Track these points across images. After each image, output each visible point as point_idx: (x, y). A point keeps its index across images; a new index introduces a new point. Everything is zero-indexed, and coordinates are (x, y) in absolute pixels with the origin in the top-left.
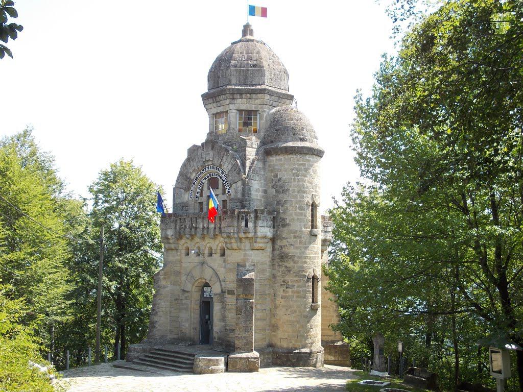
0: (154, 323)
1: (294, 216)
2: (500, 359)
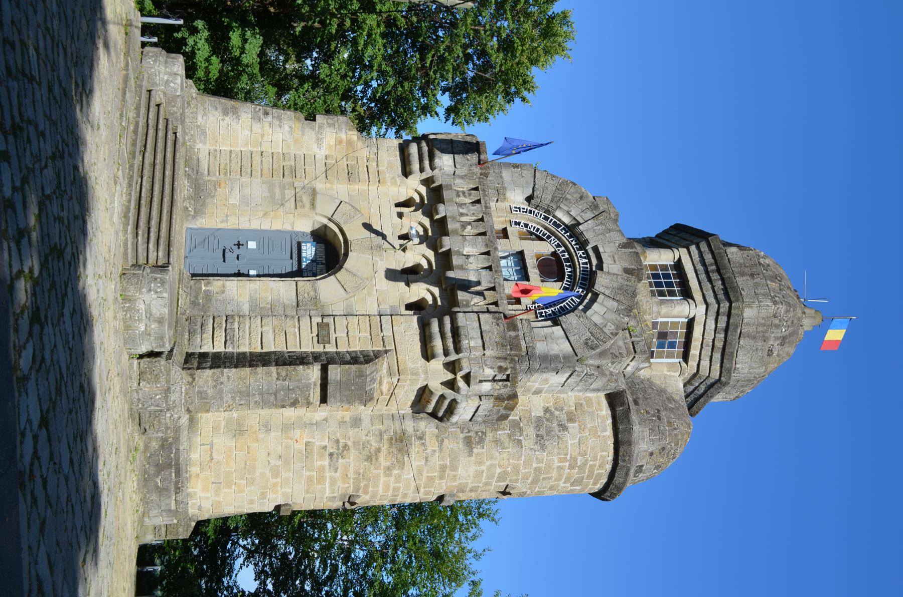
1: (488, 463)
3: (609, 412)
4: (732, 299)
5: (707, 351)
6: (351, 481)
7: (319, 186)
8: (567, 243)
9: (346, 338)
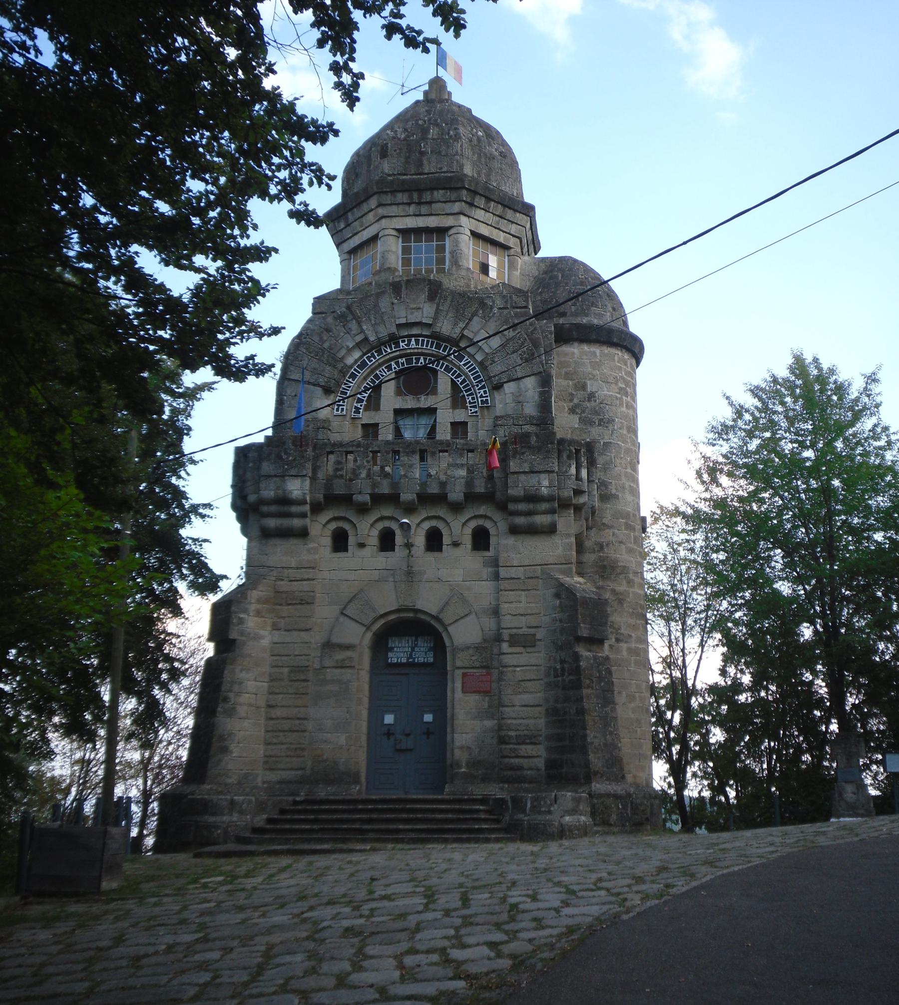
0: (225, 740)
2: (378, 859)
3: (576, 344)
4: (459, 185)
5: (503, 224)
6: (638, 622)
7: (316, 638)
8: (388, 357)
9: (527, 617)
